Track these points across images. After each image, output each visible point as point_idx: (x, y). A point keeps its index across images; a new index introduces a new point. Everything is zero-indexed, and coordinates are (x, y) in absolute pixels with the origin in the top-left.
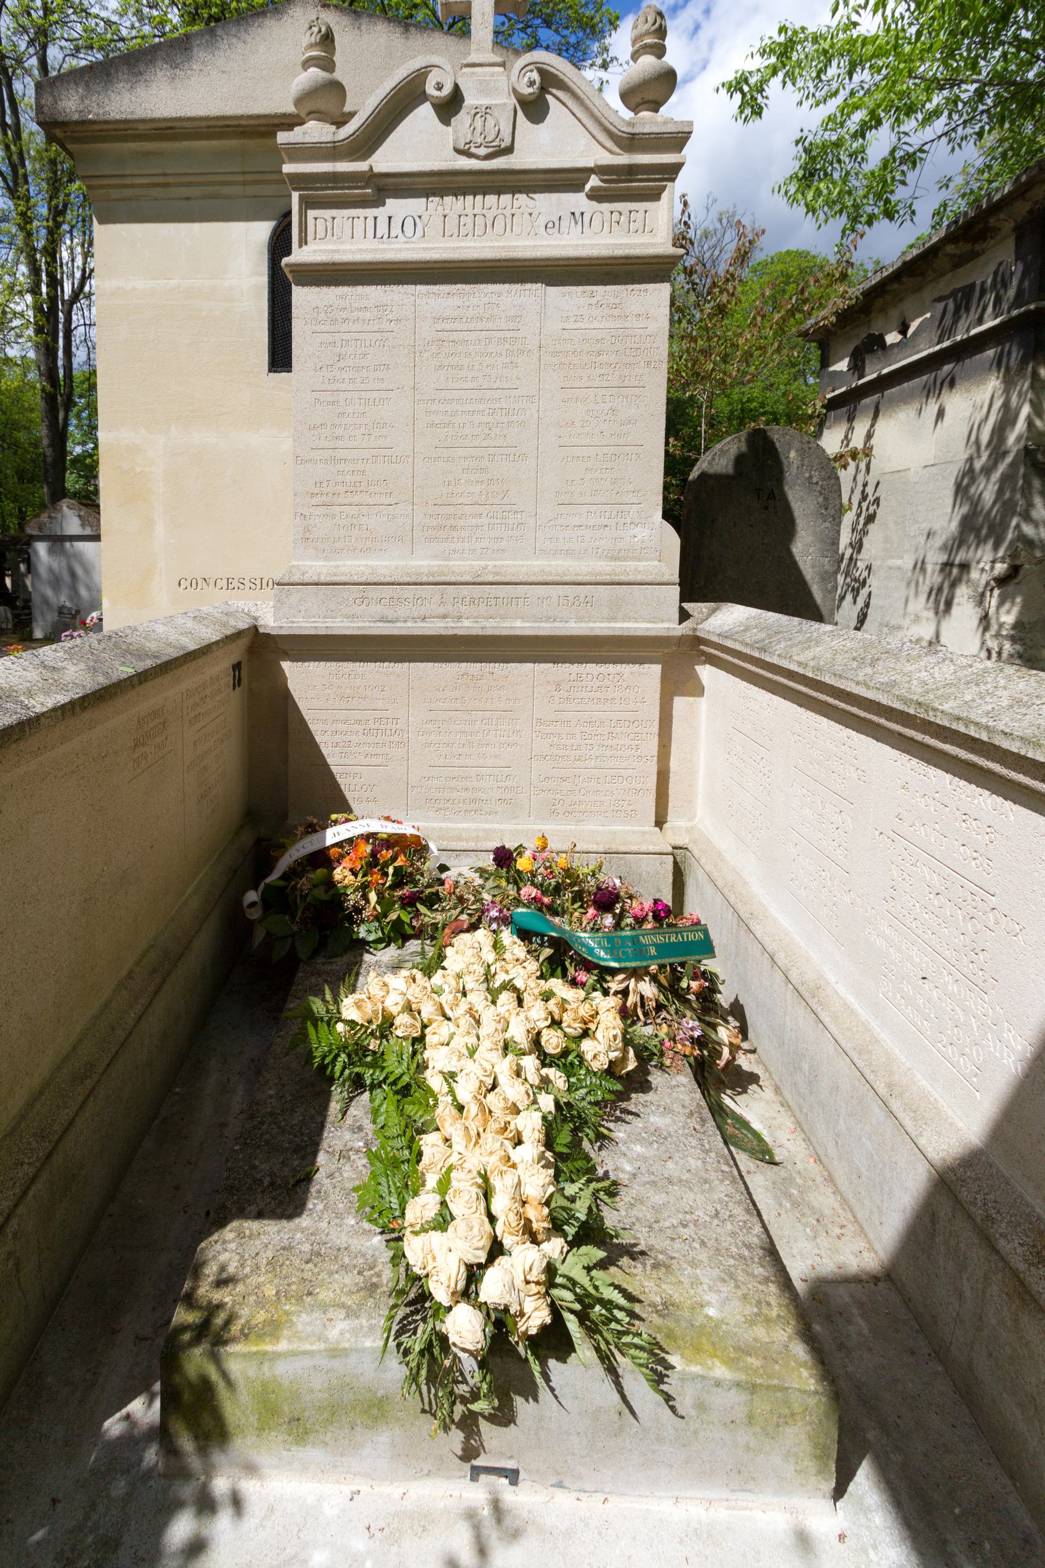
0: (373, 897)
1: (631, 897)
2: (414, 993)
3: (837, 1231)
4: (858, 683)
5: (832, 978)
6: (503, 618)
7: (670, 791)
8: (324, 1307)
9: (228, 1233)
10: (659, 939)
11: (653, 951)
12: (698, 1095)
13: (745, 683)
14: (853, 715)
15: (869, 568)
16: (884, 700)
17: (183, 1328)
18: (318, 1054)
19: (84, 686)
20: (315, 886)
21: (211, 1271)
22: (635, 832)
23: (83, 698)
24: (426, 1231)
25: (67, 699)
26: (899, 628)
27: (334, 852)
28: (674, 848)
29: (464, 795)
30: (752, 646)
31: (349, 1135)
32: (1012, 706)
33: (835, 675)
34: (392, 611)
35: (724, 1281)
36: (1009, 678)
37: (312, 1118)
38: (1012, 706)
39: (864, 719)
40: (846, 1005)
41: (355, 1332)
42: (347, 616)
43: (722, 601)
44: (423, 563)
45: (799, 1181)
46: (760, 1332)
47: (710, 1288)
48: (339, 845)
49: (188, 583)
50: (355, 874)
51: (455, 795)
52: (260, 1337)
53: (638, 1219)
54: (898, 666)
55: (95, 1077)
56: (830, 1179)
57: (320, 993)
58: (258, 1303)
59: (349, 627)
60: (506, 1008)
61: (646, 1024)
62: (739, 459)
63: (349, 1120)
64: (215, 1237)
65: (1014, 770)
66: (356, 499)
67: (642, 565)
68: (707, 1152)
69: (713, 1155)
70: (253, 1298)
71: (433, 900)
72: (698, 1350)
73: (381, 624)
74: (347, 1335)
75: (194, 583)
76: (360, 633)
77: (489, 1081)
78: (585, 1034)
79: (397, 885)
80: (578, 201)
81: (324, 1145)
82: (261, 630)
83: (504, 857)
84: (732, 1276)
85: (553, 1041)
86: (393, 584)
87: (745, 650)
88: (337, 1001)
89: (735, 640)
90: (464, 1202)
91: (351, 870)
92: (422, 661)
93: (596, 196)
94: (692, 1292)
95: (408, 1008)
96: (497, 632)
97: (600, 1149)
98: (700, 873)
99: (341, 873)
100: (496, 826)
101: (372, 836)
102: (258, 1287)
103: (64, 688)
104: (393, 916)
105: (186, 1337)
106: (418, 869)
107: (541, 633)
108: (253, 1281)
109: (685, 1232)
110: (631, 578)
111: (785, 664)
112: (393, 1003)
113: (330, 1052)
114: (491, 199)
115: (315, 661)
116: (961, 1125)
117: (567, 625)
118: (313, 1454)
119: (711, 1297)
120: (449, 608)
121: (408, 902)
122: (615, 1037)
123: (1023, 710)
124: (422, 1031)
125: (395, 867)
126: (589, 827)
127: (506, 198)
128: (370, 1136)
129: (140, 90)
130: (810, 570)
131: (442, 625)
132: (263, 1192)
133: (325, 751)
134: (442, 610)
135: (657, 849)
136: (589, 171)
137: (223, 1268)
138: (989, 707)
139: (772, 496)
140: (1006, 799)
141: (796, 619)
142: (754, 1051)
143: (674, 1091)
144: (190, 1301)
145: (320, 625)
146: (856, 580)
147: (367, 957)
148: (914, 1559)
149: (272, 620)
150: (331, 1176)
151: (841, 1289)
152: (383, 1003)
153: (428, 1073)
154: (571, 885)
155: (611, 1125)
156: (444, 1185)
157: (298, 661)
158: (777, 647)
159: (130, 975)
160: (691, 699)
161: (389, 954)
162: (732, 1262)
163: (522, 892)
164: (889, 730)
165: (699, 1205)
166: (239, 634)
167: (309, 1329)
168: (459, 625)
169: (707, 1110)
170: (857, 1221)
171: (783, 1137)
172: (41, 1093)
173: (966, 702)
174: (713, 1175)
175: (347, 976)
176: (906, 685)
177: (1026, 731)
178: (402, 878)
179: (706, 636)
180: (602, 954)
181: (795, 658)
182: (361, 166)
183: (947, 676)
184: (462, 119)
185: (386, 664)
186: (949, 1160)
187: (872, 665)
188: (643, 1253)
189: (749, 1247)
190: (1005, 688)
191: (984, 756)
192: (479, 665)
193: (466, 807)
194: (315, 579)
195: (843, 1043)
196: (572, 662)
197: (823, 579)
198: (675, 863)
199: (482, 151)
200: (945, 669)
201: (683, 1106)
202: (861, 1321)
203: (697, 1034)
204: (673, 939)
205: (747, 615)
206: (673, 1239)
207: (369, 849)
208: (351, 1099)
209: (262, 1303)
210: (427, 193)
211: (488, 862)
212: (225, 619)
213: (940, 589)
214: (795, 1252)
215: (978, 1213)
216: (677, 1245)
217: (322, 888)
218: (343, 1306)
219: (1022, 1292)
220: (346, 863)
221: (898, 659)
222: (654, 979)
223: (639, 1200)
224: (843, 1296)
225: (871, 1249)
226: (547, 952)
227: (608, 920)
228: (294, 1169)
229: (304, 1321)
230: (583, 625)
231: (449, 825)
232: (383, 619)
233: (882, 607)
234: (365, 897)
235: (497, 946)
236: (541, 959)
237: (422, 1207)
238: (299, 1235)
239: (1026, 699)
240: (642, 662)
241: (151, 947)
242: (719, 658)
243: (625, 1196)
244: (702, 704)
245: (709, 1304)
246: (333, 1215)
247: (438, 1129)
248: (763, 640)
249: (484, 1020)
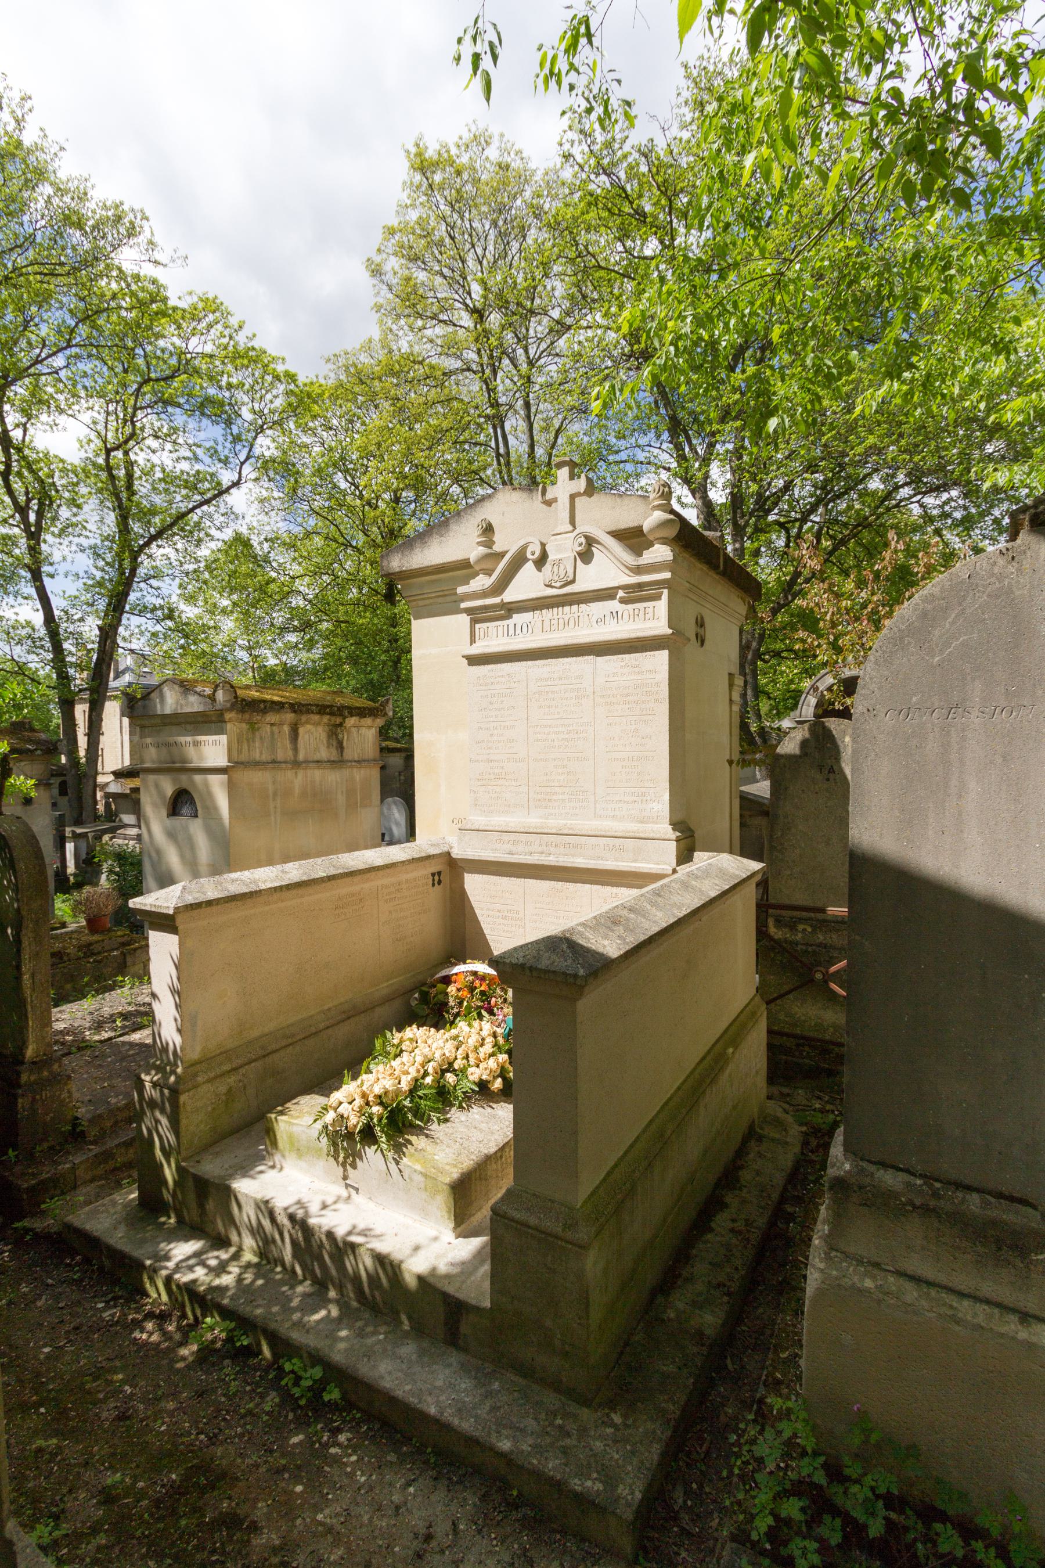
6: (573, 856)
44: (534, 820)
62: (804, 744)
66: (500, 782)
67: (656, 827)
80: (614, 605)
93: (623, 601)
114: (567, 609)
118: (303, 1164)
127: (575, 607)
129: (426, 552)
134: (540, 849)
136: (619, 588)
139: (831, 770)
159: (329, 1009)
182: (497, 600)
184: (547, 567)
199: (558, 584)
210: (534, 609)
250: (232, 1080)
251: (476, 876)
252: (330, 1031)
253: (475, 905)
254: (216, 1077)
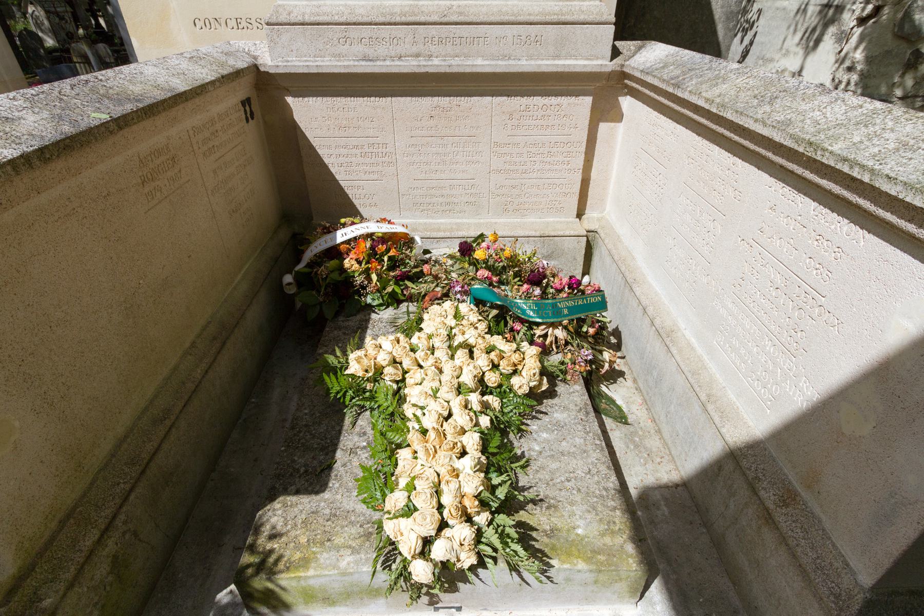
0: (374, 277)
1: (554, 276)
2: (398, 352)
3: (659, 460)
4: (756, 121)
5: (682, 325)
6: (467, 56)
7: (590, 193)
8: (338, 548)
9: (277, 505)
10: (571, 304)
11: (566, 312)
12: (586, 397)
13: (656, 113)
14: (744, 146)
15: (760, 11)
16: (777, 137)
17: (248, 566)
18: (334, 391)
19: (42, 137)
20: (332, 272)
21: (266, 530)
22: (563, 222)
23: (41, 150)
24: (396, 517)
25: (16, 154)
26: (771, 60)
27: (343, 248)
28: (588, 232)
29: (441, 200)
30: (667, 82)
31: (356, 441)
32: (898, 150)
33: (737, 112)
34: (372, 50)
35: (589, 512)
36: (896, 120)
37: (333, 427)
38: (898, 150)
39: (753, 151)
40: (689, 345)
41: (357, 563)
42: (334, 55)
43: (646, 39)
45: (640, 433)
46: (608, 540)
47: (581, 517)
48: (348, 242)
49: (202, 23)
50: (360, 263)
51: (434, 200)
52: (297, 568)
53: (540, 480)
54: (794, 105)
55: (173, 418)
56: (659, 431)
57: (333, 353)
58: (295, 547)
59: (336, 66)
60: (461, 360)
61: (557, 353)
63: (357, 429)
64: (268, 507)
65: (883, 209)
68: (587, 433)
69: (591, 435)
70: (292, 544)
71: (416, 277)
72: (569, 554)
73: (363, 63)
74: (352, 565)
75: (207, 23)
76: (346, 71)
77: (446, 414)
78: (515, 372)
79: (392, 268)
81: (341, 445)
82: (262, 69)
83: (466, 249)
84: (594, 508)
85: (492, 379)
86: (370, 24)
87: (663, 86)
88: (345, 354)
89: (654, 76)
90: (423, 501)
91: (356, 260)
92: (402, 96)
94: (569, 521)
95: (394, 362)
96: (461, 70)
97: (520, 438)
98: (603, 248)
99: (349, 263)
100: (465, 220)
101: (370, 235)
102: (296, 537)
103: (17, 141)
104: (389, 289)
105: (250, 571)
106: (407, 256)
107: (498, 70)
108: (293, 533)
109: (568, 485)
110: (575, 18)
111: (694, 99)
112: (383, 359)
113: (341, 390)
115: (313, 96)
116: (751, 424)
117: (519, 63)
119: (581, 523)
120: (419, 48)
121: (399, 280)
122: (534, 375)
123: (909, 155)
124: (403, 376)
125: (389, 257)
126: (531, 219)
128: (371, 438)
130: (719, 10)
131: (415, 63)
132: (300, 477)
133: (333, 170)
134: (415, 49)
135: (576, 233)
137: (274, 527)
138: (876, 150)
140: (862, 228)
141: (708, 57)
142: (623, 358)
143: (573, 394)
144: (252, 549)
145: (311, 64)
146: (747, 21)
147: (373, 316)
148: (673, 613)
149: (269, 59)
150: (344, 465)
151: (656, 492)
152: (375, 359)
153: (405, 406)
154: (514, 267)
155: (529, 422)
156: (411, 488)
157: (298, 97)
158: (689, 84)
159: (193, 345)
160: (613, 124)
161: (387, 314)
162: (595, 499)
163: (478, 274)
164: (772, 162)
165: (579, 466)
166: (237, 74)
167: (328, 562)
168: (430, 63)
169: (590, 406)
170: (671, 454)
171: (634, 408)
172: (126, 437)
173: (854, 144)
174: (589, 447)
175: (357, 334)
176: (800, 124)
177: (911, 177)
178: (394, 264)
179: (631, 72)
180: (531, 313)
181: (704, 94)
183: (838, 116)
185: (373, 99)
186: (739, 444)
187: (771, 103)
188: (541, 500)
189: (606, 489)
190: (892, 130)
191: (857, 194)
192: (448, 98)
193: (443, 208)
194: (300, 19)
195: (683, 367)
196: (522, 96)
197: (728, 19)
198: (588, 241)
200: (836, 109)
201: (576, 405)
202: (665, 509)
203: (590, 357)
204: (580, 303)
205: (666, 53)
206: (561, 490)
207: (368, 244)
208: (359, 414)
209: (298, 547)
211: (455, 250)
212: (224, 58)
213: (814, 30)
214: (632, 473)
215: (751, 475)
216: (563, 493)
217: (337, 272)
218: (350, 547)
219: (768, 518)
220: (352, 255)
221: (794, 98)
222: (565, 328)
223: (542, 468)
224: (657, 496)
225: (677, 469)
226: (494, 312)
227: (538, 291)
228: (321, 462)
229: (325, 557)
230: (533, 62)
231: (431, 221)
232: (366, 58)
233: (762, 43)
234: (369, 279)
235: (457, 316)
236: (490, 317)
237: (396, 500)
238: (323, 504)
239: (912, 142)
240: (577, 95)
241: (209, 323)
242: (638, 90)
243: (534, 466)
244: (620, 128)
245: (579, 527)
246: (343, 491)
247: (409, 445)
248: (678, 77)
249: (445, 369)
250: (111, 546)
253: (315, 142)
254: (80, 570)
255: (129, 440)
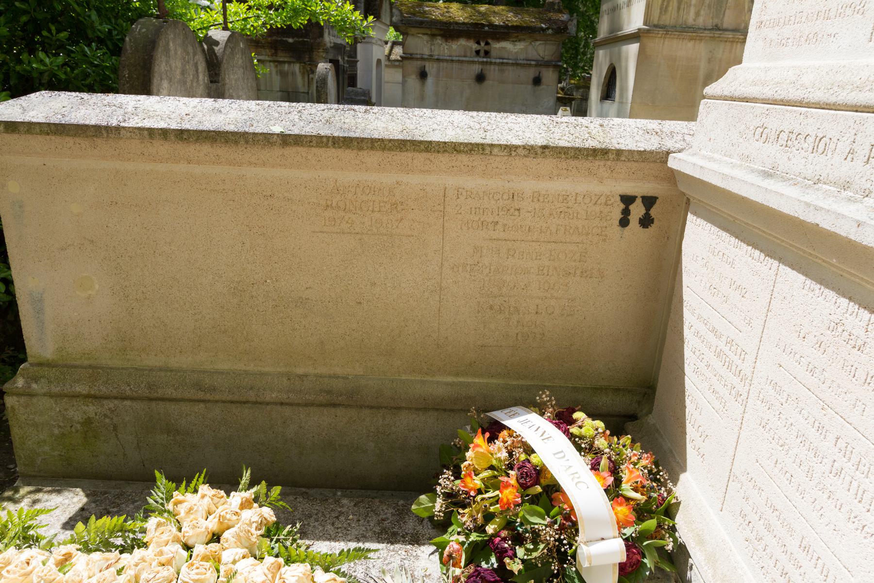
159: (302, 377)
250: (91, 409)
251: (700, 221)
252: (287, 411)
254: (60, 396)
255: (169, 374)
